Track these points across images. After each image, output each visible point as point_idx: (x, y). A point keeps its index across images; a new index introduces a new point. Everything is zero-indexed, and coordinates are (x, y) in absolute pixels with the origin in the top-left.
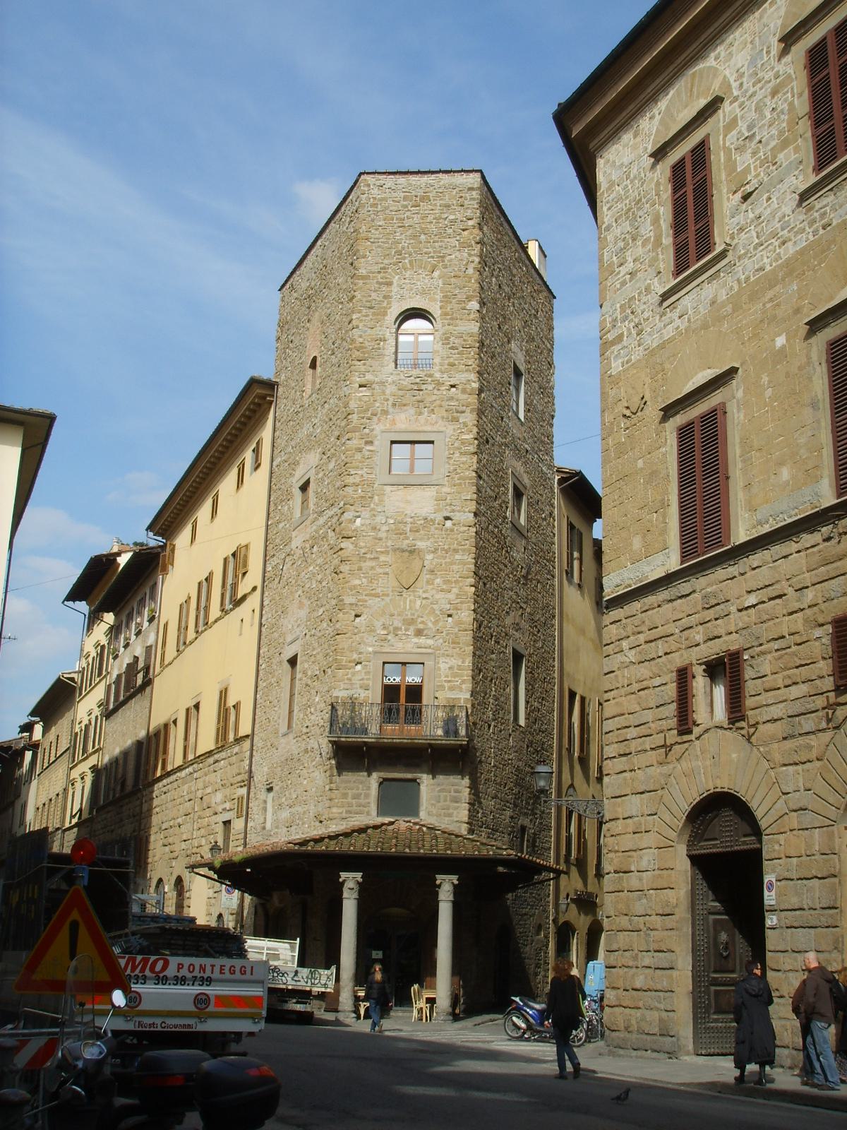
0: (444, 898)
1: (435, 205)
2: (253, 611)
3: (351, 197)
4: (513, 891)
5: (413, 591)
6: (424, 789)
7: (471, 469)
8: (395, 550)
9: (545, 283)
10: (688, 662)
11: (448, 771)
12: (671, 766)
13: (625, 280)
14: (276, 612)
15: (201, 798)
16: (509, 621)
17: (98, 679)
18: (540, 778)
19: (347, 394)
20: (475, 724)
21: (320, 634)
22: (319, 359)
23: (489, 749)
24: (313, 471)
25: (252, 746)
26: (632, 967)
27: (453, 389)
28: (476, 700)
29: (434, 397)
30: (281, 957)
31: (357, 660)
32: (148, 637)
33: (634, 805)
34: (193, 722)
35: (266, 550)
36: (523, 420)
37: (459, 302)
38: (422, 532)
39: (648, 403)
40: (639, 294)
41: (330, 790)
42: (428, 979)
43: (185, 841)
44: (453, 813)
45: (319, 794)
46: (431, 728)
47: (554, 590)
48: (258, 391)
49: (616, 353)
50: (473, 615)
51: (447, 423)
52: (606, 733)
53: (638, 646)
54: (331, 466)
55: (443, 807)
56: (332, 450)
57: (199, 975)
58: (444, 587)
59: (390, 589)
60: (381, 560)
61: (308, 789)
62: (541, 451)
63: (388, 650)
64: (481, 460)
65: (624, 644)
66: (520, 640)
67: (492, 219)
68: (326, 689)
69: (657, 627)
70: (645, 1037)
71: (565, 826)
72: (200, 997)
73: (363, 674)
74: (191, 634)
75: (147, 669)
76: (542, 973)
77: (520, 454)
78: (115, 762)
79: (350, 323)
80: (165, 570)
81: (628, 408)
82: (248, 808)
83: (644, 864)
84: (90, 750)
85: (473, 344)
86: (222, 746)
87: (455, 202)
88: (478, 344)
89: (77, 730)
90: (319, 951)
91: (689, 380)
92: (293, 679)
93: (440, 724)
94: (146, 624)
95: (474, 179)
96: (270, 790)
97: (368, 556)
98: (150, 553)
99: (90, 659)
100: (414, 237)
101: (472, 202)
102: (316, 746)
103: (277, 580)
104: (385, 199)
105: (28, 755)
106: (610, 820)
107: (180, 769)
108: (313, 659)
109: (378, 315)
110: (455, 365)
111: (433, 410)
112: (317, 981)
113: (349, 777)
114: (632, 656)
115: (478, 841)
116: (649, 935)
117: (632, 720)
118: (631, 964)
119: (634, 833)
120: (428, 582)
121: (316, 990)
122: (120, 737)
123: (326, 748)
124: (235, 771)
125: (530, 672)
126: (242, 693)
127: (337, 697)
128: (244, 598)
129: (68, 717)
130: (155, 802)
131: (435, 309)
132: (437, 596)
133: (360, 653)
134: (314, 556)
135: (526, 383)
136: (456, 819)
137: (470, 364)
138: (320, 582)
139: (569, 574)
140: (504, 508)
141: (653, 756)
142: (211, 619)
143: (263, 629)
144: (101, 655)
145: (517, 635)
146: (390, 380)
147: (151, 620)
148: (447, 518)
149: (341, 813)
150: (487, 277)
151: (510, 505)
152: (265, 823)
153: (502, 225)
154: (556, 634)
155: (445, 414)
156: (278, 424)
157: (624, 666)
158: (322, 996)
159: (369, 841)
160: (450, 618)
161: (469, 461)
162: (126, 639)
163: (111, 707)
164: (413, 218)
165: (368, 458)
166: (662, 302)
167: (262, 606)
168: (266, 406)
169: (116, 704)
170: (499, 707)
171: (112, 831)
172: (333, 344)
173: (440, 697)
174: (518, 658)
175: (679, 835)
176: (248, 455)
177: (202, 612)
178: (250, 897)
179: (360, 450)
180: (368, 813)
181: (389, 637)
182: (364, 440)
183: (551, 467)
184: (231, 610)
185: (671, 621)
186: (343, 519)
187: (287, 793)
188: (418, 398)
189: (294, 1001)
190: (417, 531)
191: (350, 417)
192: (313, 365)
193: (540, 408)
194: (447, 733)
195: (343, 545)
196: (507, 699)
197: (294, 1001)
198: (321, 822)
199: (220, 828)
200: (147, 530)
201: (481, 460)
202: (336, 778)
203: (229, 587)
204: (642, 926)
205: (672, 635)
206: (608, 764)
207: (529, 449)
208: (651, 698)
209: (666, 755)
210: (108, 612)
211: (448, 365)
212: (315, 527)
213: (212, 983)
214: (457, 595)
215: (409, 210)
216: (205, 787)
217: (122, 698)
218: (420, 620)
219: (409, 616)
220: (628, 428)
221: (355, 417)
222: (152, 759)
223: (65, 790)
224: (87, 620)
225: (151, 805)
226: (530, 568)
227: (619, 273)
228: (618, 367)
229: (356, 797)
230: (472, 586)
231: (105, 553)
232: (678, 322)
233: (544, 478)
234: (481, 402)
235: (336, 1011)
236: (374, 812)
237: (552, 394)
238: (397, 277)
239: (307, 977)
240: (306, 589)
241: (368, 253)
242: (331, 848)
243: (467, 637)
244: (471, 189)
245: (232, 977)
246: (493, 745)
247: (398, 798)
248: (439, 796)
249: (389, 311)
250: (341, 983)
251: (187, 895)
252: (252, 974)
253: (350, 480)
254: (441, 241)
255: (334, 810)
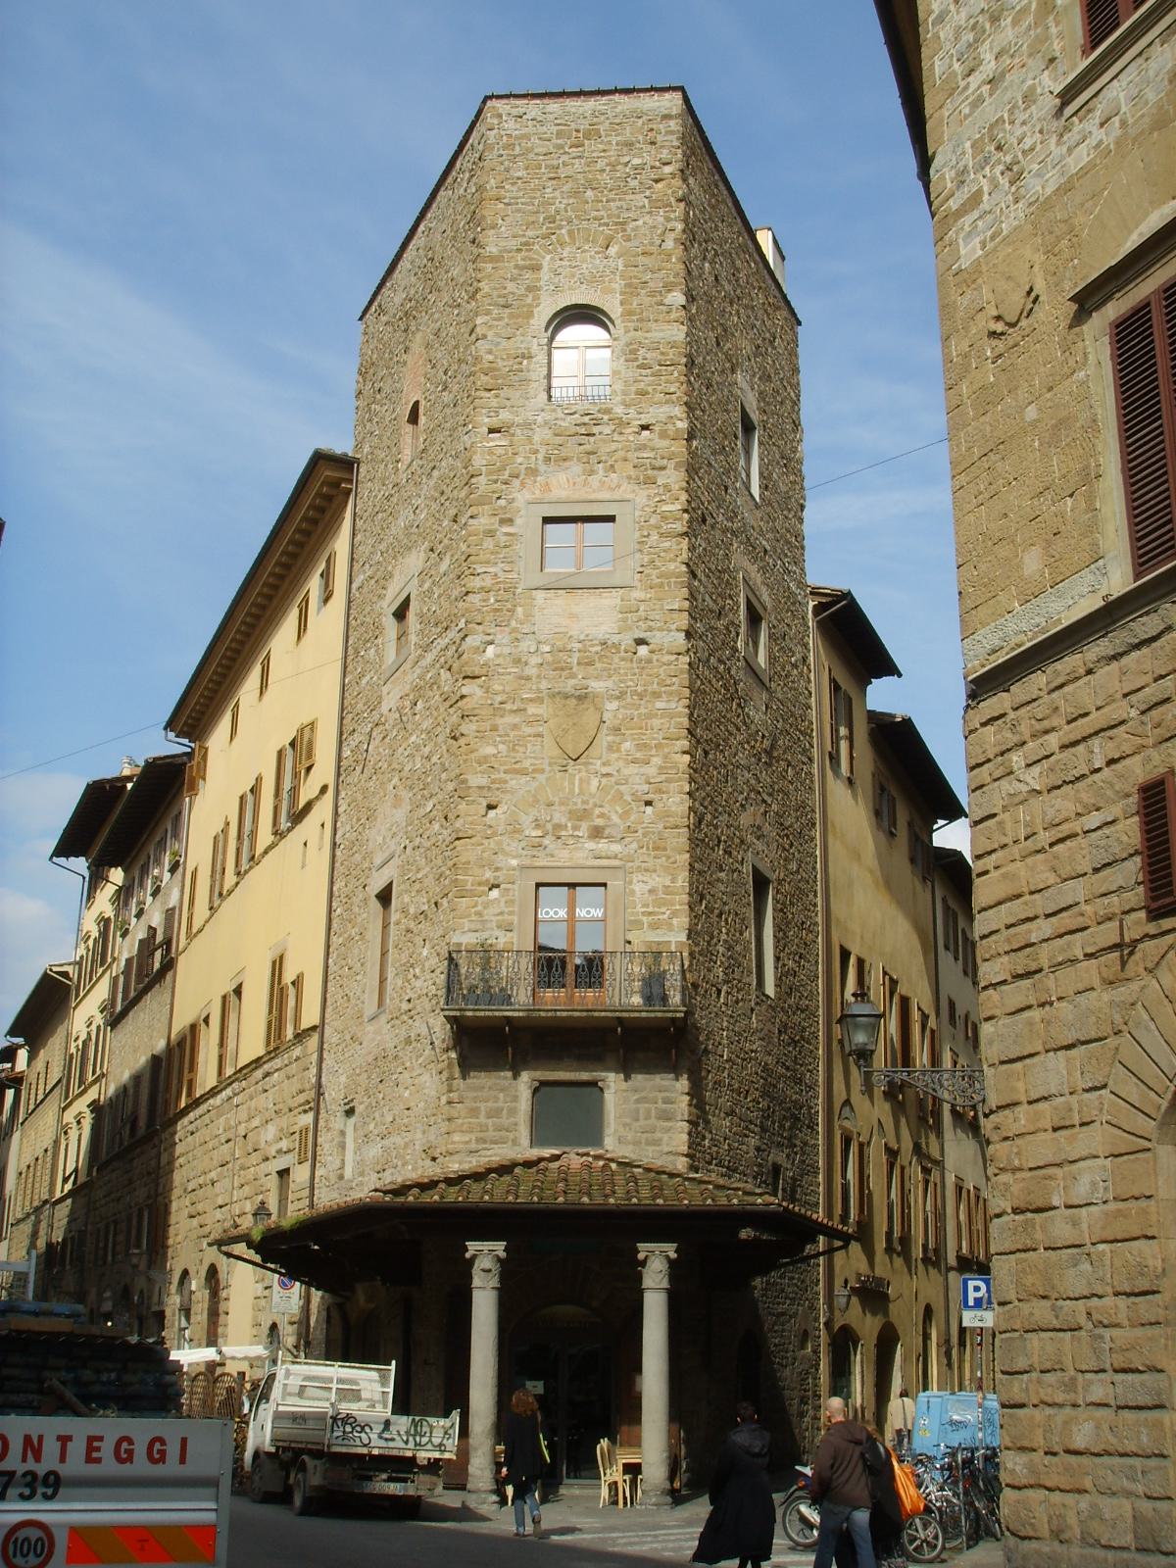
0: (652, 1285)
1: (609, 143)
2: (323, 825)
3: (471, 141)
4: (765, 1272)
5: (586, 764)
6: (610, 1098)
7: (679, 559)
8: (553, 696)
9: (784, 297)
10: (1162, 770)
11: (649, 1068)
12: (1135, 986)
13: (981, 95)
14: (359, 820)
15: (245, 1137)
16: (745, 819)
17: (100, 971)
18: (857, 1026)
19: (468, 446)
20: (695, 986)
21: (428, 844)
22: (423, 403)
23: (719, 1029)
24: (415, 581)
25: (322, 1042)
26: (1060, 1406)
27: (646, 433)
28: (697, 945)
29: (614, 446)
30: (364, 1395)
31: (492, 881)
32: (169, 895)
33: (1053, 1072)
34: (232, 1017)
35: (341, 725)
36: (758, 499)
37: (652, 294)
38: (598, 665)
39: (1040, 299)
40: (1011, 112)
41: (449, 1103)
42: (624, 1428)
43: (221, 1207)
44: (661, 1140)
45: (429, 1113)
46: (623, 994)
47: (812, 781)
48: (328, 473)
49: (967, 228)
50: (688, 803)
51: (636, 487)
52: (983, 937)
53: (1047, 757)
54: (444, 567)
55: (643, 1127)
56: (446, 541)
57: (21, 1469)
58: (638, 755)
59: (547, 761)
60: (530, 713)
61: (412, 1104)
62: (786, 556)
63: (546, 864)
64: (694, 548)
65: (1015, 759)
66: (763, 855)
67: (701, 170)
68: (441, 932)
69: (1086, 714)
70: (1099, 1553)
71: (839, 1160)
72: (21, 1534)
73: (502, 904)
74: (230, 878)
75: (168, 943)
76: (811, 1413)
77: (756, 553)
78: (123, 1091)
79: (472, 331)
80: (193, 789)
81: (998, 318)
82: (315, 1145)
83: (1081, 1191)
84: (90, 1078)
85: (677, 359)
86: (276, 1049)
87: (641, 138)
88: (685, 360)
89: (73, 1050)
90: (430, 1386)
91: (1130, 232)
92: (385, 926)
93: (637, 985)
94: (167, 876)
95: (672, 102)
96: (350, 1112)
97: (508, 707)
98: (170, 764)
99: (91, 943)
100: (576, 194)
101: (670, 137)
102: (424, 1031)
103: (359, 769)
104: (527, 137)
105: (10, 1094)
106: (999, 1108)
107: (213, 1092)
108: (417, 886)
109: (518, 316)
110: (647, 393)
111: (612, 466)
112: (425, 1440)
113: (481, 1079)
114: (1034, 778)
115: (709, 1183)
116: (1101, 1337)
117: (1041, 904)
118: (1060, 1398)
119: (1055, 1130)
120: (610, 748)
121: (423, 1456)
122: (127, 1057)
123: (441, 1030)
124: (295, 1086)
125: (780, 910)
126: (306, 962)
127: (461, 944)
128: (309, 806)
129: (61, 1031)
130: (179, 1149)
131: (612, 306)
132: (626, 771)
133: (497, 869)
134: (417, 717)
135: (761, 443)
136: (666, 1149)
137: (672, 390)
138: (428, 758)
139: (834, 758)
140: (733, 634)
141: (1090, 972)
142: (259, 850)
143: (338, 853)
144: (104, 934)
145: (759, 845)
146: (539, 419)
147: (173, 869)
148: (640, 642)
149: (467, 1143)
150: (696, 257)
151: (743, 630)
152: (342, 1167)
153: (717, 186)
154: (818, 853)
155: (633, 473)
156: (359, 523)
157: (1017, 800)
158: (434, 1466)
159: (518, 1186)
160: (649, 809)
161: (674, 547)
162: (139, 903)
163: (119, 1008)
164: (573, 164)
165: (506, 547)
166: (1064, 104)
167: (336, 814)
168: (341, 497)
169: (126, 1003)
170: (734, 964)
171: (118, 1200)
172: (445, 373)
173: (635, 941)
174: (761, 883)
175: (1162, 1125)
176: (314, 585)
177: (246, 843)
178: (320, 1293)
179: (491, 534)
180: (515, 1142)
181: (546, 841)
182: (497, 518)
183: (802, 585)
184: (289, 830)
185: (1119, 696)
186: (464, 646)
187: (377, 1115)
188: (587, 447)
189: (384, 1476)
190: (591, 664)
191: (473, 480)
192: (414, 418)
193: (783, 488)
194: (648, 999)
195: (464, 691)
196: (747, 949)
197: (384, 1476)
198: (434, 1159)
199: (273, 1182)
200: (165, 728)
201: (694, 548)
202: (458, 1083)
203: (285, 796)
204: (1082, 1320)
205: (1123, 722)
206: (989, 998)
207: (768, 548)
208: (1080, 854)
209: (1124, 964)
210: (116, 867)
211: (637, 393)
212: (418, 671)
213: (61, 1491)
214: (661, 768)
215: (565, 153)
216: (251, 1118)
217: (132, 994)
218: (597, 811)
219: (580, 806)
220: (1000, 356)
221: (482, 479)
222: (175, 1082)
223: (57, 1142)
224: (86, 884)
225: (172, 1154)
226: (775, 741)
227: (966, 88)
228: (974, 250)
229: (494, 1113)
230: (684, 752)
231: (109, 777)
232: (1099, 135)
233: (793, 604)
234: (692, 454)
235: (463, 1488)
236: (525, 1141)
237: (800, 471)
238: (548, 257)
239: (408, 1433)
240: (404, 774)
241: (500, 221)
242: (450, 1199)
243: (680, 839)
244: (667, 117)
245: (126, 1470)
246: (725, 1024)
247: (567, 1115)
248: (637, 1111)
249: (536, 310)
250: (471, 1441)
251: (224, 1294)
252: (183, 1460)
253: (475, 583)
254: (620, 200)
255: (456, 1137)
